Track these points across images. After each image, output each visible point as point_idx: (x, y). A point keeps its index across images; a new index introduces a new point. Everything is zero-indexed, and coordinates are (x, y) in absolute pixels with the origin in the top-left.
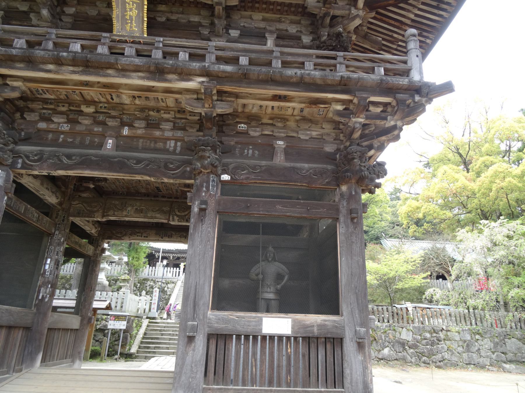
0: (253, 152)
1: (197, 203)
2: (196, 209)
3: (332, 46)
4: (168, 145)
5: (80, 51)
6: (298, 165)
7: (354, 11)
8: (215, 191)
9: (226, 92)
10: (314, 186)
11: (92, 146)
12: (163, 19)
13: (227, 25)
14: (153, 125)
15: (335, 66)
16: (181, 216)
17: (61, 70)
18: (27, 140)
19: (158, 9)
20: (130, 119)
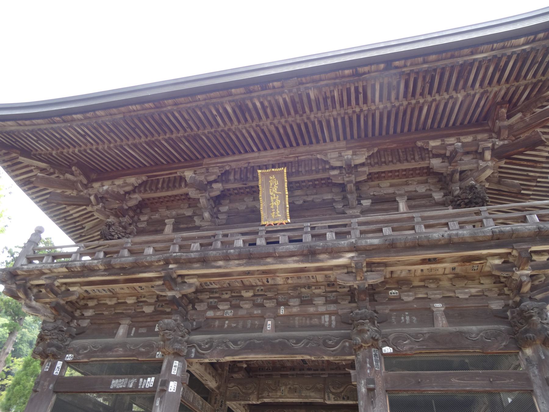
0: (410, 318)
1: (363, 382)
2: (363, 390)
3: (468, 198)
4: (323, 320)
5: (242, 245)
6: (465, 328)
7: (482, 164)
8: (379, 366)
9: (374, 263)
10: (489, 351)
11: (253, 329)
12: (301, 202)
13: (357, 197)
14: (306, 302)
15: (481, 221)
16: (336, 393)
17: (229, 264)
18: (197, 330)
19: (296, 194)
20: (285, 298)
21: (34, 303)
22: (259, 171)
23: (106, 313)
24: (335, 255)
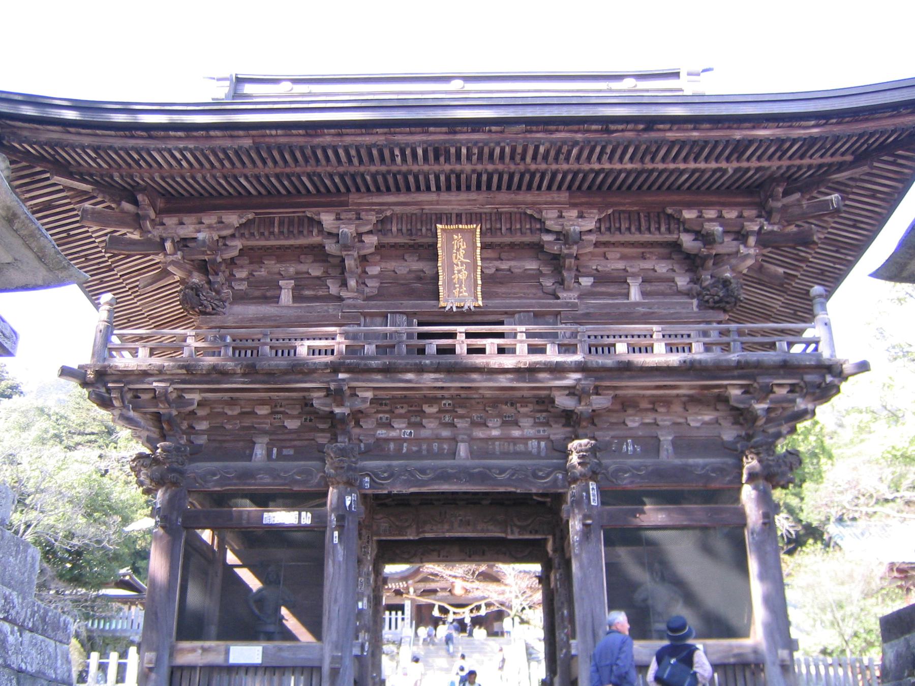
6: (691, 461)
7: (742, 249)
11: (439, 455)
20: (481, 417)
21: (132, 413)
22: (439, 226)
23: (228, 427)
24: (558, 375)
